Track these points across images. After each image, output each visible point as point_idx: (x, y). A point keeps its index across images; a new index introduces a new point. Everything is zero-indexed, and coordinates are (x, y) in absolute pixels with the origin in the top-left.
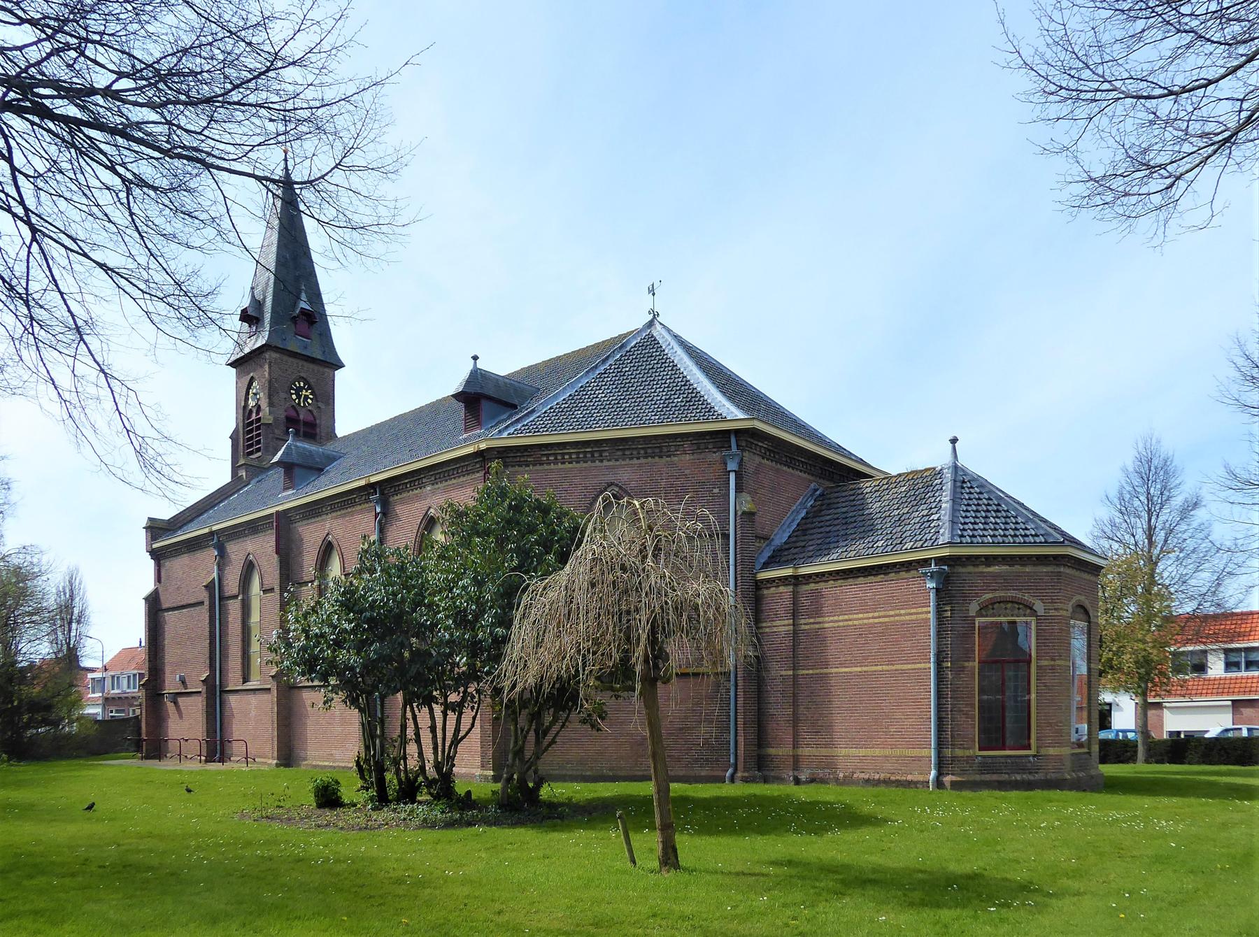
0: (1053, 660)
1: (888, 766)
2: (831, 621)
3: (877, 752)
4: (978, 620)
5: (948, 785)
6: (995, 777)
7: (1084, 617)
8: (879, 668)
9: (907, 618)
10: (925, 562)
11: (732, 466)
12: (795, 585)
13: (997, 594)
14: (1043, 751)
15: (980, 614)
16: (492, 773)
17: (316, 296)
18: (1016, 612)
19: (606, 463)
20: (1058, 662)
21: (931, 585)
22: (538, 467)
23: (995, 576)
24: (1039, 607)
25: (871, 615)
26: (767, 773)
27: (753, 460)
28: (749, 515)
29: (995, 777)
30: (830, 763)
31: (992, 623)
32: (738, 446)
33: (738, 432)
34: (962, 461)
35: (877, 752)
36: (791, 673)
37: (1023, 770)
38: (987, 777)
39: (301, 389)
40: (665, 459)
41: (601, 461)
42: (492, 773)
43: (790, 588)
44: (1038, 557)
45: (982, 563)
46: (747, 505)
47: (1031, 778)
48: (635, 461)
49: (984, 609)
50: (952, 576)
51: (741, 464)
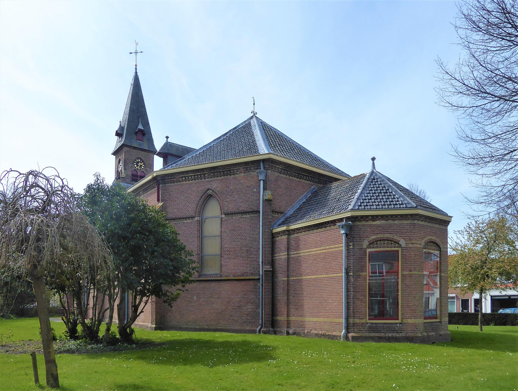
0: (410, 271)
1: (326, 327)
2: (304, 252)
3: (321, 319)
4: (368, 250)
5: (350, 338)
6: (377, 335)
7: (437, 248)
8: (322, 276)
9: (334, 250)
10: (341, 220)
11: (262, 177)
12: (289, 235)
13: (379, 236)
14: (405, 321)
15: (369, 247)
16: (154, 326)
17: (146, 124)
18: (390, 245)
19: (207, 179)
20: (413, 272)
21: (343, 232)
22: (179, 183)
23: (378, 226)
24: (402, 242)
25: (319, 249)
26: (276, 329)
27: (273, 174)
28: (268, 202)
29: (377, 335)
30: (302, 325)
31: (375, 251)
32: (264, 168)
33: (264, 161)
34: (378, 169)
35: (321, 319)
36: (286, 279)
37: (394, 331)
38: (373, 334)
39: (139, 162)
40: (232, 176)
41: (205, 179)
42: (154, 326)
43: (286, 237)
44: (402, 215)
45: (370, 220)
46: (268, 195)
47: (397, 335)
48: (219, 178)
49: (371, 244)
50: (353, 226)
51: (266, 175)
